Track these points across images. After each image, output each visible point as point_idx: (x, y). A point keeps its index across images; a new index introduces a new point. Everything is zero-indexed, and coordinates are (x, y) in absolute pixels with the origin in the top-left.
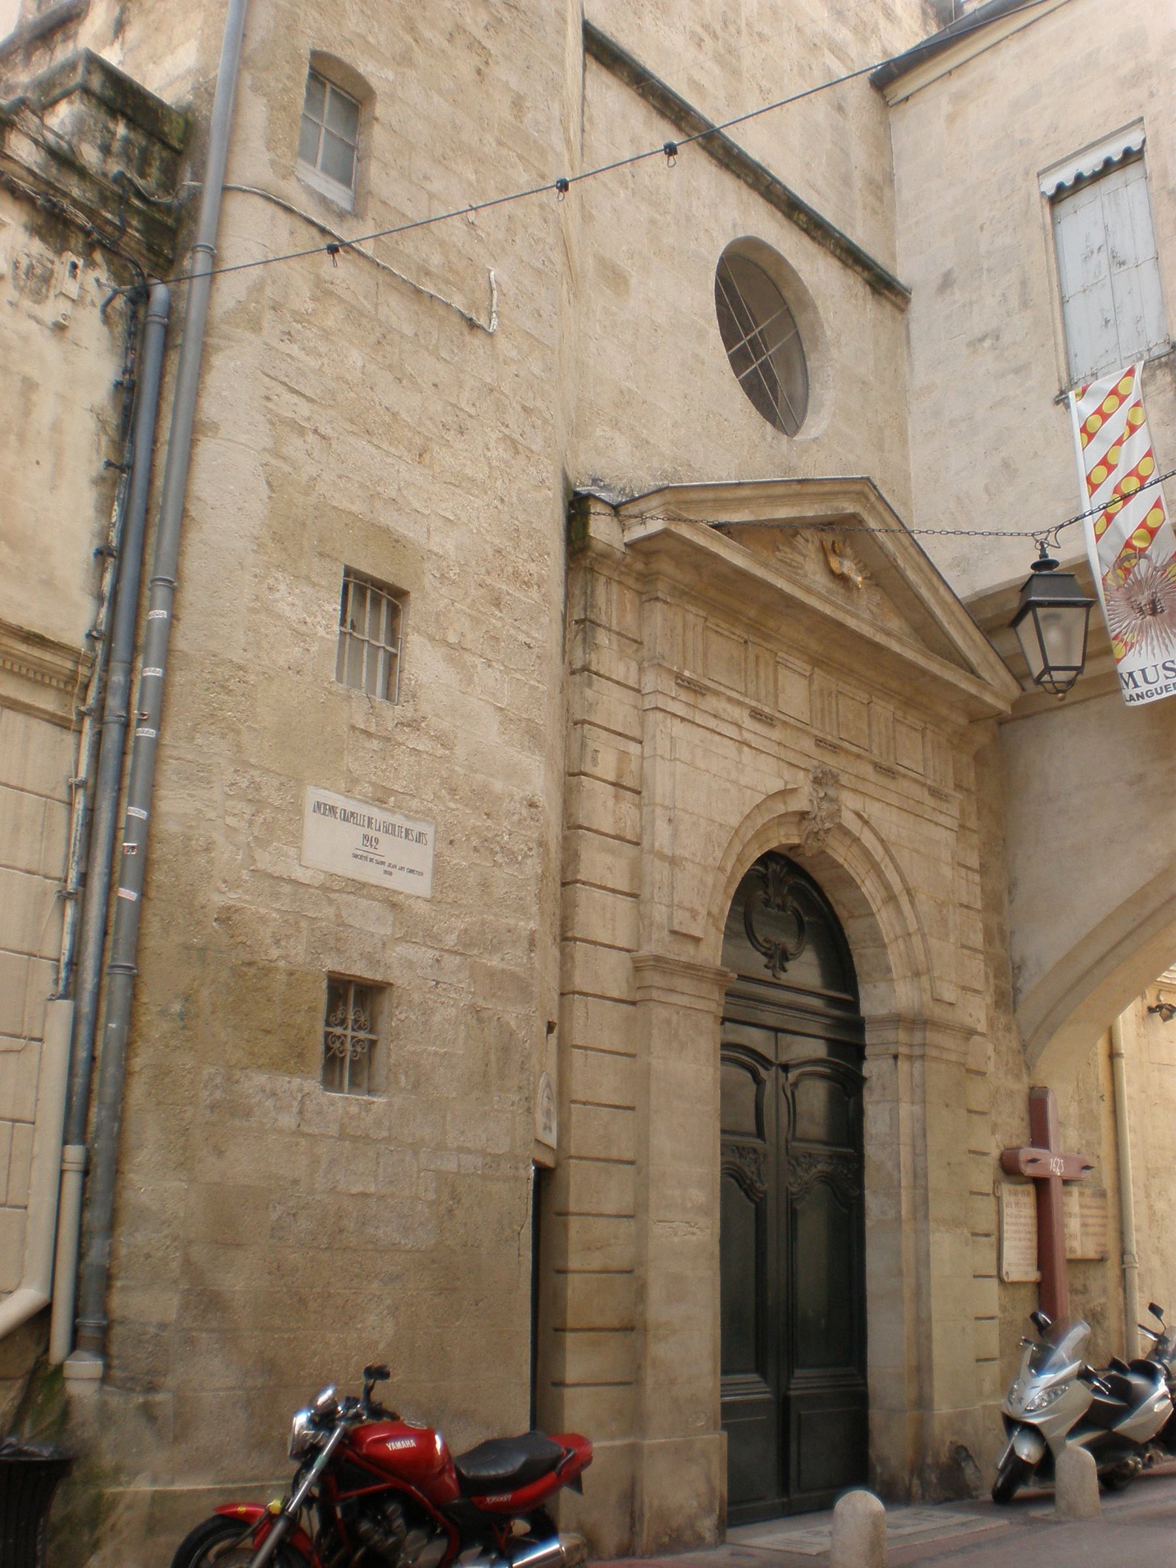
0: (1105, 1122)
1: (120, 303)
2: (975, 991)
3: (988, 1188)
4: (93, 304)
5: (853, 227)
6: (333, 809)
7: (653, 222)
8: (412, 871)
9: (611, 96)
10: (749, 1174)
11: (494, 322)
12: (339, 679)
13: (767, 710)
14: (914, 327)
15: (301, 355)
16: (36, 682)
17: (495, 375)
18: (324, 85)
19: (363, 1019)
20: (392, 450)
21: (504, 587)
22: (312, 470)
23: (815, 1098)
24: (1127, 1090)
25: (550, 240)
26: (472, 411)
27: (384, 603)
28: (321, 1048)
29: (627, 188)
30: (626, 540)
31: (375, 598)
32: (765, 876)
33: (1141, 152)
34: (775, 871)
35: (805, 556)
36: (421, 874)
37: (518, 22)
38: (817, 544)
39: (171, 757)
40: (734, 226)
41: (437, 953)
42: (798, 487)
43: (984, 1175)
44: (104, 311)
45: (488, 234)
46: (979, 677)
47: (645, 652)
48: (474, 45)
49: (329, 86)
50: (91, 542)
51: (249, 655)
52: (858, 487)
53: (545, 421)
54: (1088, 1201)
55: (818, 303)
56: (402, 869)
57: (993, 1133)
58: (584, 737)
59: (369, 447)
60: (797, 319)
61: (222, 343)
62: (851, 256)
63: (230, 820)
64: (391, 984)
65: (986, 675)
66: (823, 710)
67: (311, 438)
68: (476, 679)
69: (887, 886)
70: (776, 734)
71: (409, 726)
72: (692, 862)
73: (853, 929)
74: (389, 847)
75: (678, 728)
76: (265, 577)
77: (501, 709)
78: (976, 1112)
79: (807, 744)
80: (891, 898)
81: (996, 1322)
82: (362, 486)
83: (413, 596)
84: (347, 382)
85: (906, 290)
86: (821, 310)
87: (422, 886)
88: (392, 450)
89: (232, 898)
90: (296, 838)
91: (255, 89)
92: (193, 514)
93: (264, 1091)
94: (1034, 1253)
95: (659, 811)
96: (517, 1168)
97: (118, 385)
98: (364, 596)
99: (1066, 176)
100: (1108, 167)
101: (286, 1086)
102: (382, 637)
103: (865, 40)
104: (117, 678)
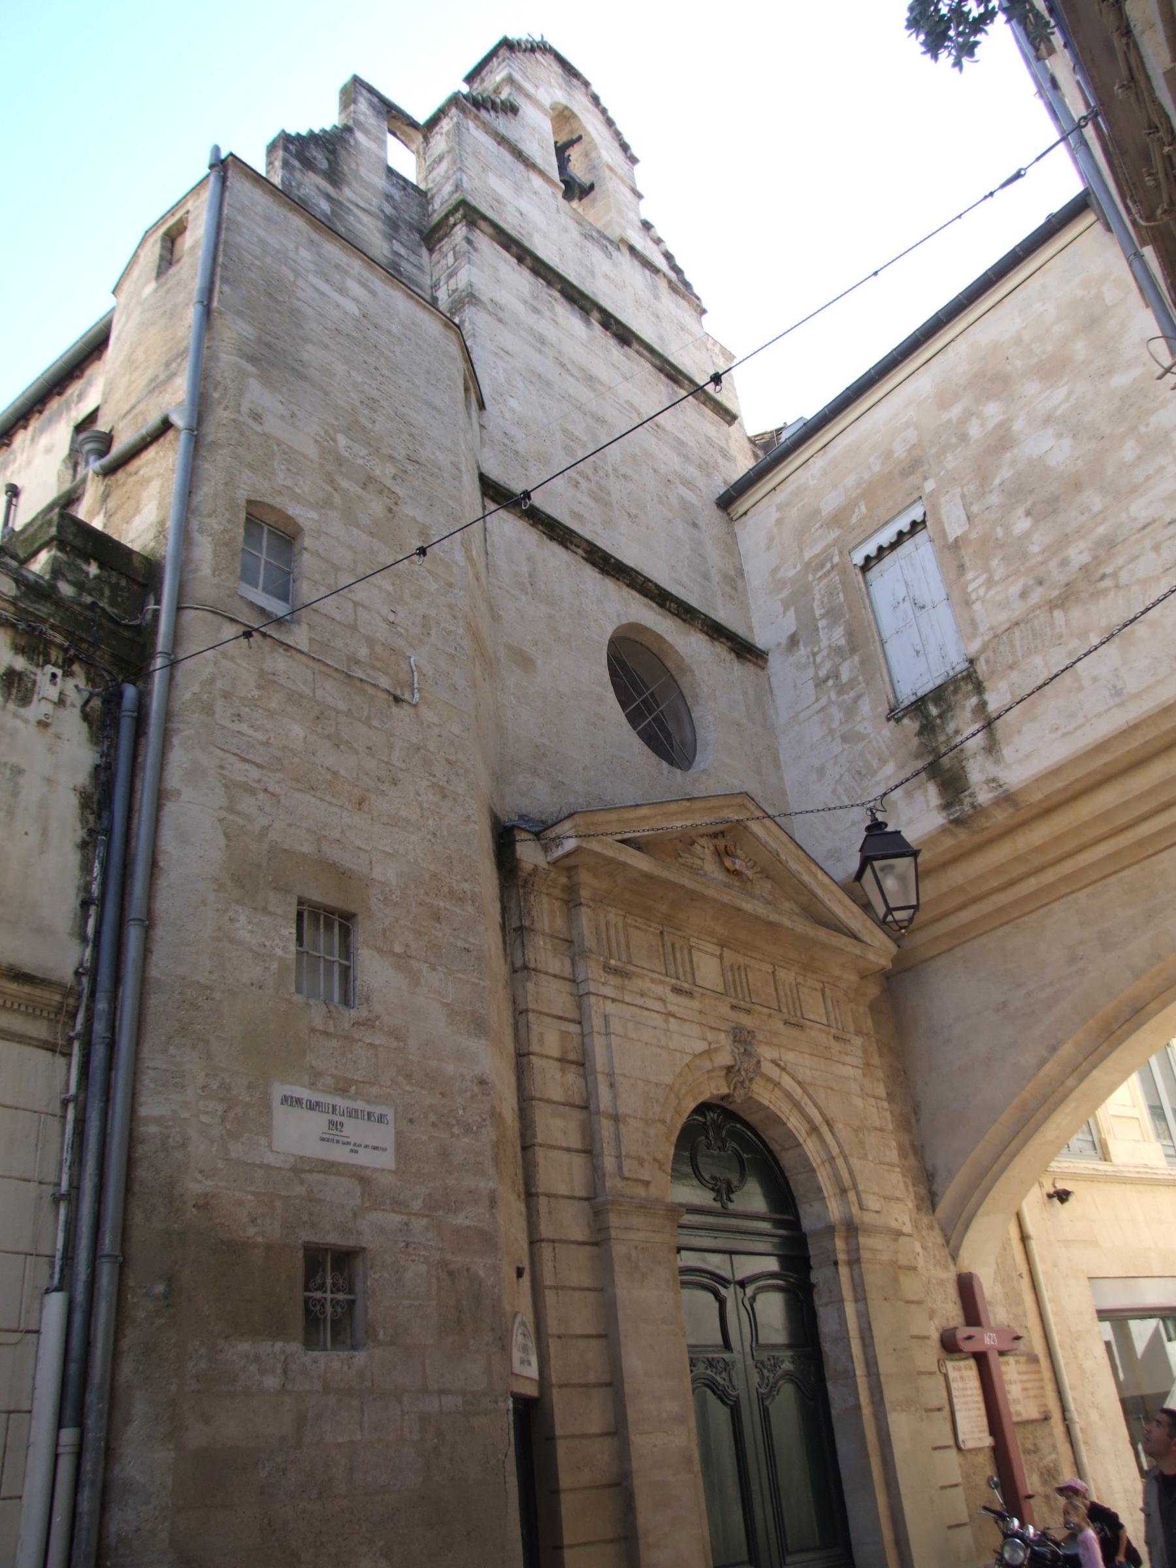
0: (1028, 1297)
1: (96, 703)
2: (898, 1199)
3: (935, 1368)
4: (73, 706)
5: (715, 610)
6: (299, 1101)
7: (551, 617)
8: (375, 1148)
9: (507, 527)
10: (722, 1382)
11: (417, 696)
12: (299, 990)
13: (686, 986)
15: (250, 732)
16: (28, 1015)
17: (420, 737)
18: (262, 528)
19: (341, 1282)
20: (334, 801)
21: (442, 904)
22: (264, 821)
23: (772, 1309)
24: (1040, 1268)
25: (460, 631)
26: (403, 766)
27: (336, 924)
28: (300, 1312)
29: (527, 593)
30: (549, 859)
31: (329, 923)
32: (705, 1124)
33: (924, 522)
34: (712, 1119)
35: (703, 859)
36: (385, 1150)
37: (421, 473)
38: (712, 848)
39: (148, 1068)
40: (619, 616)
41: (405, 1218)
42: (687, 804)
43: (928, 1356)
44: (83, 710)
45: (407, 630)
46: (861, 941)
48: (383, 490)
49: (266, 528)
50: (77, 895)
51: (215, 976)
52: (739, 800)
53: (467, 771)
54: (1023, 1368)
55: (694, 667)
56: (366, 1146)
57: (931, 1318)
59: (313, 800)
60: (679, 682)
61: (182, 726)
62: (716, 631)
63: (203, 1118)
64: (364, 1249)
65: (867, 939)
66: (734, 981)
67: (261, 796)
68: (423, 981)
69: (809, 1121)
70: (695, 1004)
71: (364, 1025)
72: (635, 1118)
73: (787, 1160)
74: (353, 1129)
75: (610, 1007)
76: (226, 910)
77: (448, 1004)
78: (912, 1302)
79: (725, 1010)
80: (814, 1130)
81: (960, 1488)
82: (308, 830)
83: (360, 918)
84: (291, 750)
85: (763, 652)
86: (696, 672)
87: (387, 1160)
88: (334, 801)
89: (209, 1185)
90: (267, 1129)
92: (161, 864)
93: (248, 1356)
94: (984, 1421)
95: (600, 1078)
96: (496, 1402)
97: (97, 767)
98: (319, 920)
99: (870, 549)
100: (901, 536)
101: (269, 1350)
102: (336, 952)
103: (709, 475)
104: (102, 1005)
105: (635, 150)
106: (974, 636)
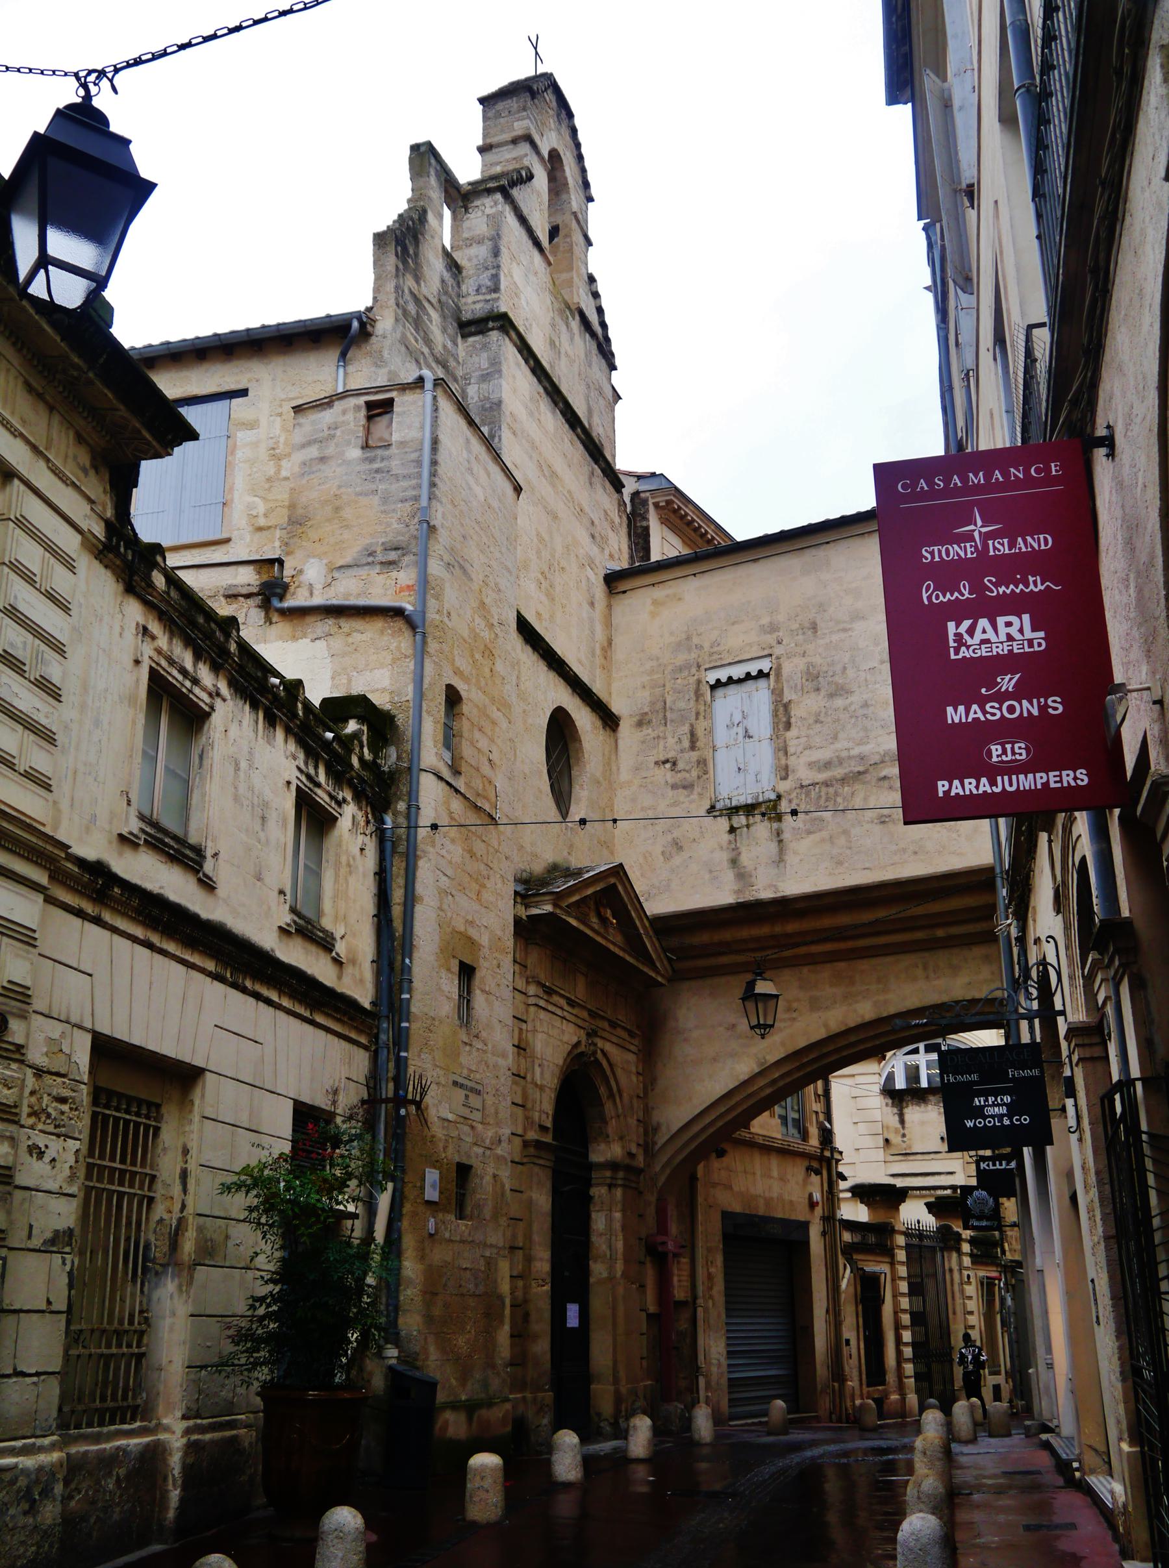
14: (620, 742)
47: (528, 973)
58: (111, 823)
79: (585, 1015)
80: (611, 1096)
91: (428, 712)
99: (723, 675)
100: (748, 677)
105: (594, 191)
106: (785, 778)
